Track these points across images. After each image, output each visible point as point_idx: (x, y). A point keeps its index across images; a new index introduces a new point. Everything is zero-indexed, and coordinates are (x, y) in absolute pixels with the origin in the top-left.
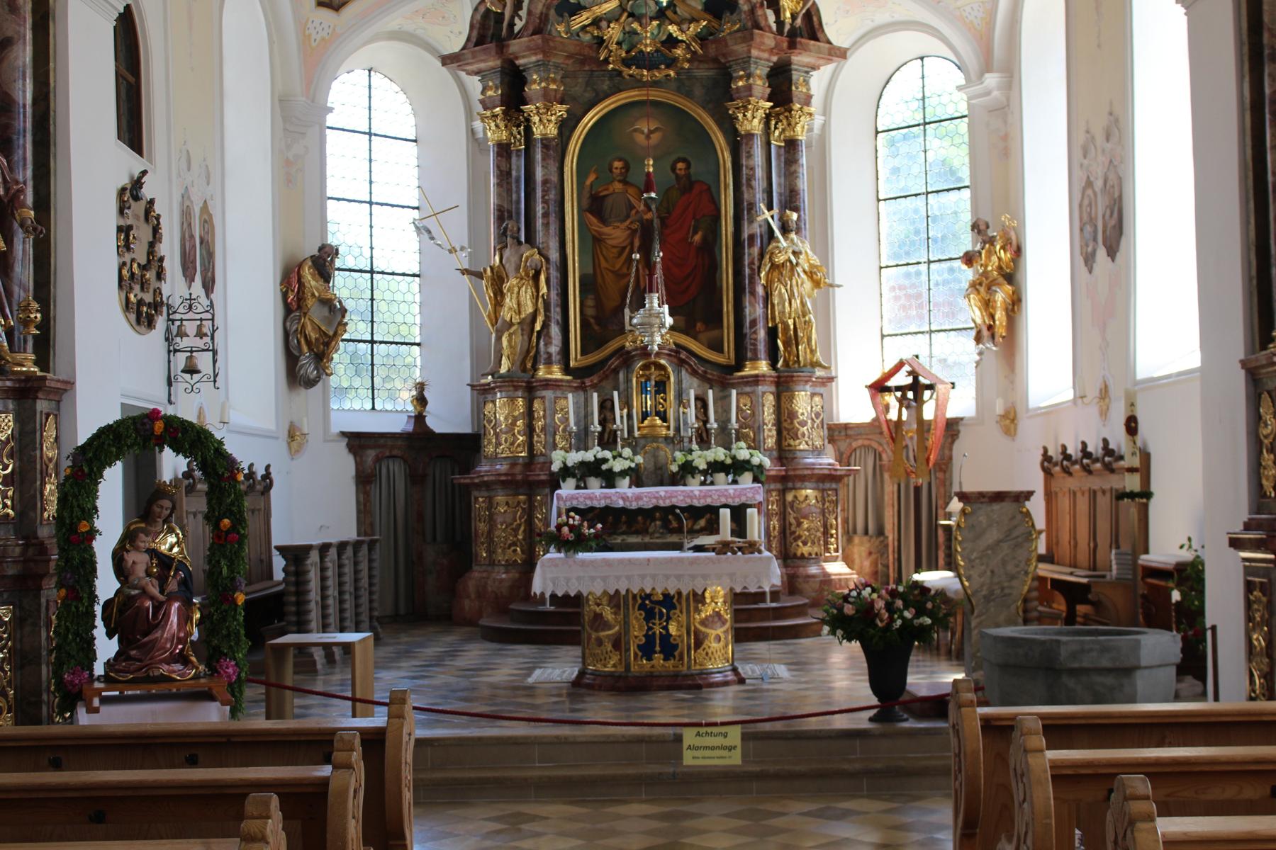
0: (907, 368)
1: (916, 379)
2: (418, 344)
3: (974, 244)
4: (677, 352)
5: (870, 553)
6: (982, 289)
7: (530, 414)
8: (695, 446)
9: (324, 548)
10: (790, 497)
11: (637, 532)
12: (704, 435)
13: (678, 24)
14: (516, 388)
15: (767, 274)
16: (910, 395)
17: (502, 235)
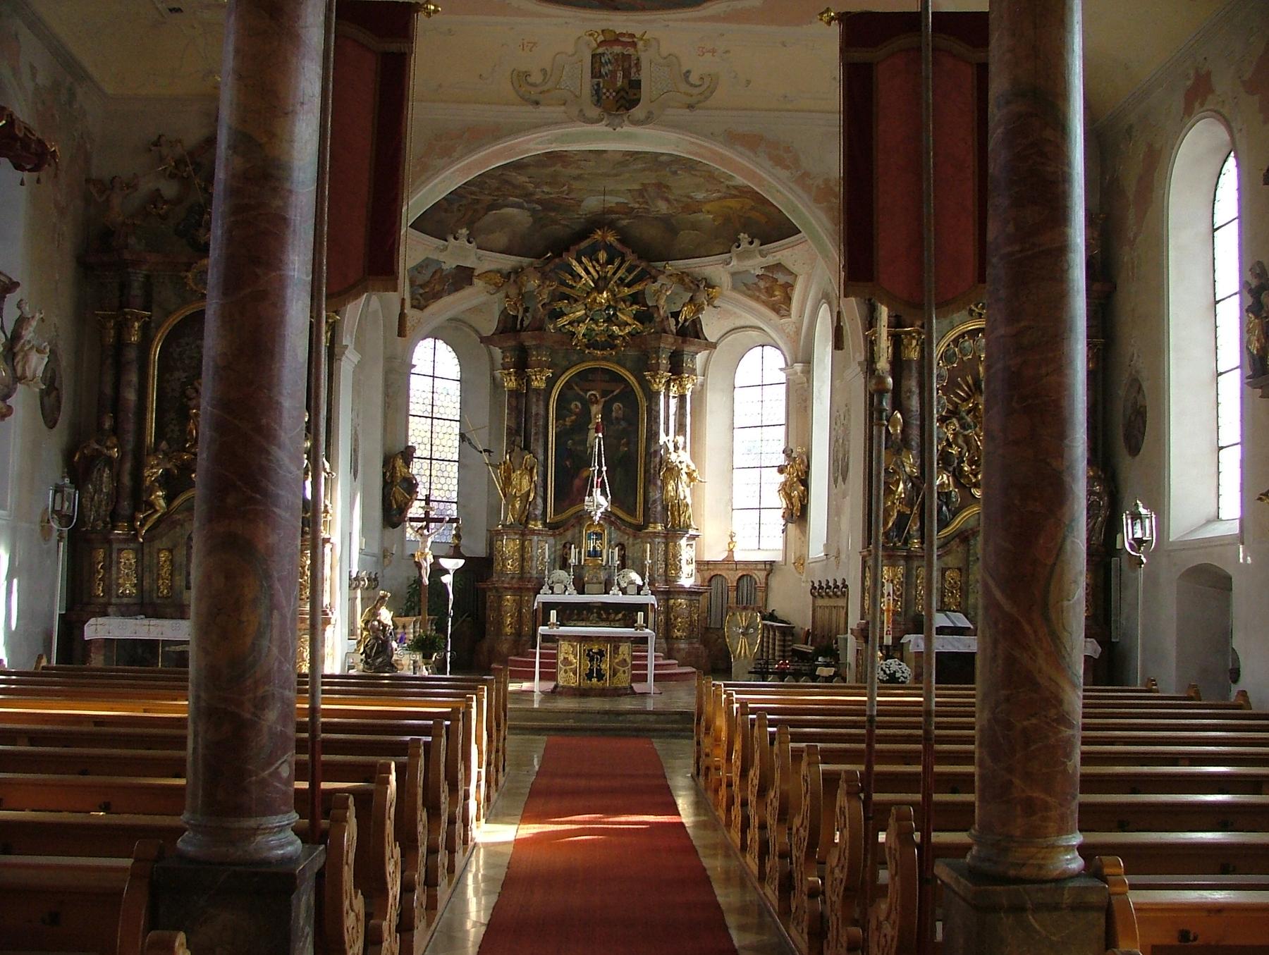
7: (523, 546)
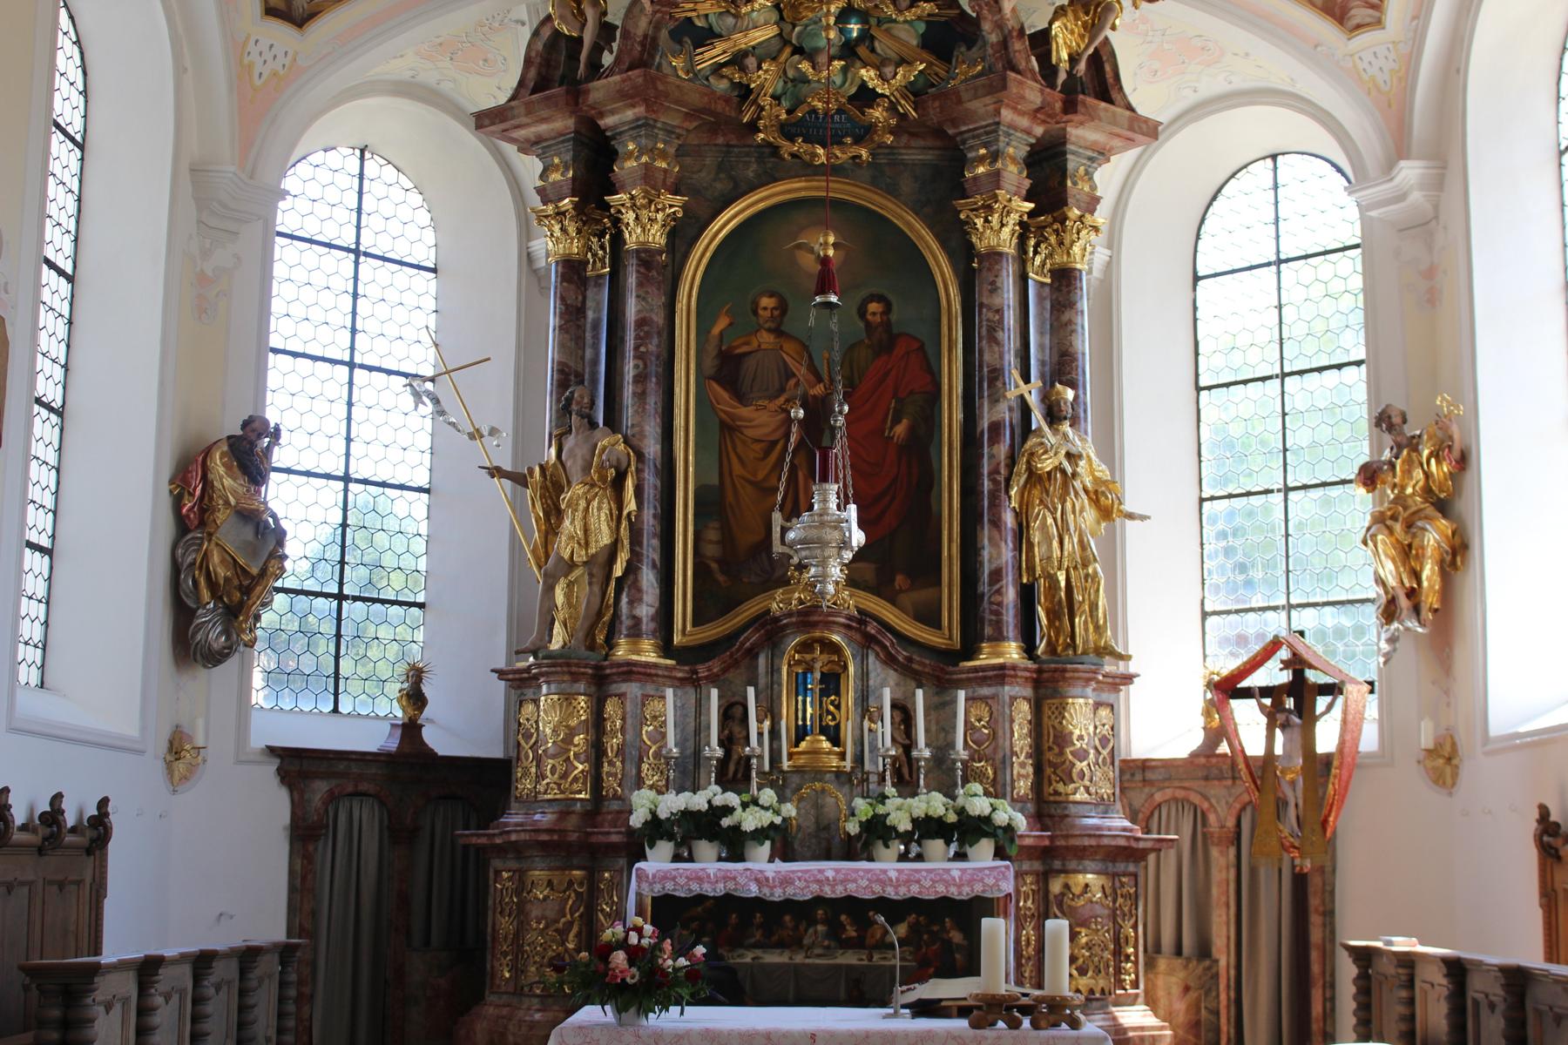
0: (1284, 653)
1: (1299, 676)
2: (421, 606)
3: (1377, 447)
4: (861, 622)
5: (1187, 989)
6: (1398, 527)
7: (598, 722)
8: (890, 790)
9: (202, 962)
10: (1056, 887)
11: (781, 945)
12: (905, 771)
13: (877, 68)
14: (575, 677)
15: (1022, 493)
16: (1290, 703)
17: (564, 409)
